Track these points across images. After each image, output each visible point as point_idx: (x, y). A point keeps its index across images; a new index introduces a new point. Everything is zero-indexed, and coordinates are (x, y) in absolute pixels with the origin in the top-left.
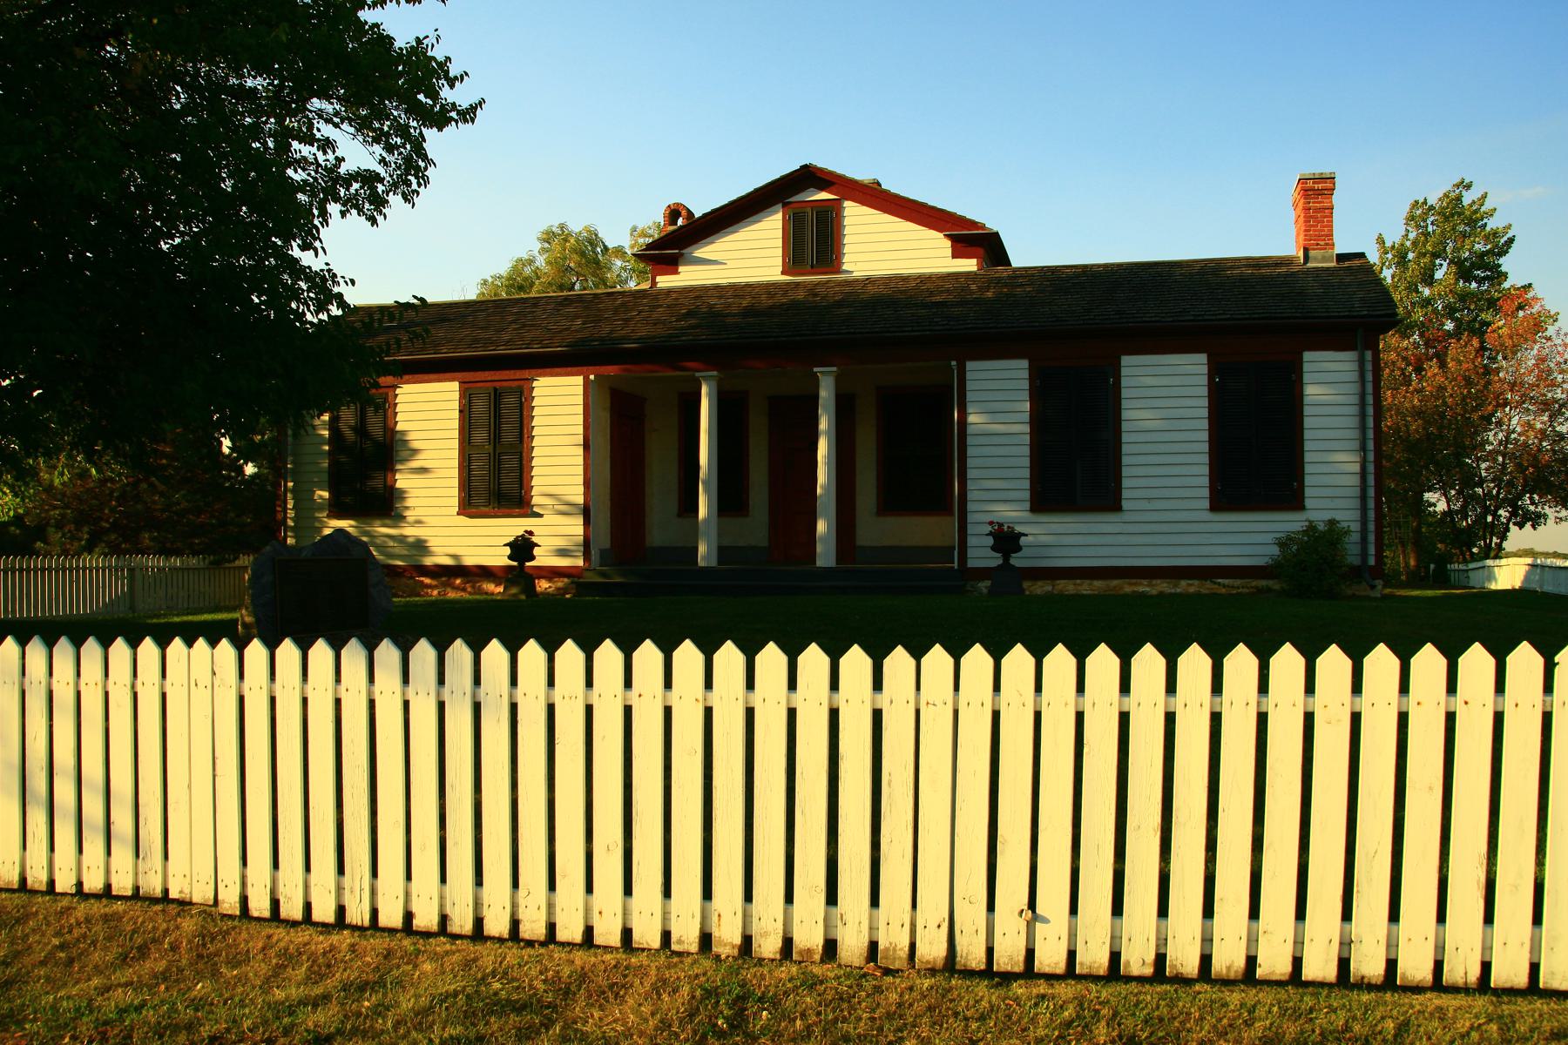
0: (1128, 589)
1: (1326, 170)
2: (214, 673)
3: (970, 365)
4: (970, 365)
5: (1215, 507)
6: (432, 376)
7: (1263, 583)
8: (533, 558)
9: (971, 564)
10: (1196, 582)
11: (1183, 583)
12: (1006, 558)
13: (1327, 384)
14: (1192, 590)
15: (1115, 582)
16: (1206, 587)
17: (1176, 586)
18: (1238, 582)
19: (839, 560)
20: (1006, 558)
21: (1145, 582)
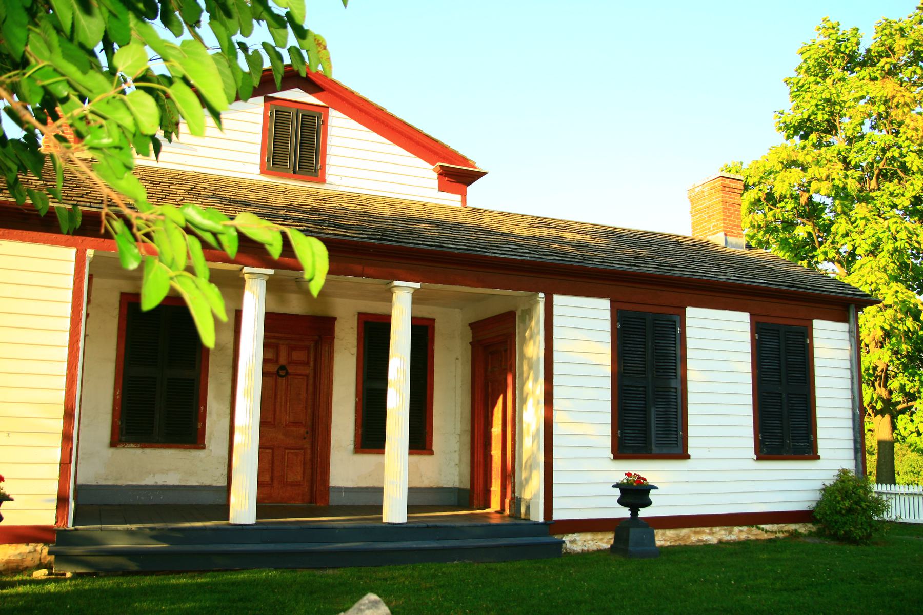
0: (694, 538)
1: (113, 450)
2: (9, 433)
3: (558, 299)
4: (558, 299)
5: (759, 458)
6: (16, 232)
7: (792, 527)
8: (648, 503)
9: (557, 516)
10: (745, 528)
11: (736, 529)
12: (634, 512)
13: (828, 341)
14: (743, 536)
15: (684, 532)
16: (739, 533)
17: (730, 533)
18: (775, 527)
19: (259, 515)
20: (634, 512)
21: (707, 530)
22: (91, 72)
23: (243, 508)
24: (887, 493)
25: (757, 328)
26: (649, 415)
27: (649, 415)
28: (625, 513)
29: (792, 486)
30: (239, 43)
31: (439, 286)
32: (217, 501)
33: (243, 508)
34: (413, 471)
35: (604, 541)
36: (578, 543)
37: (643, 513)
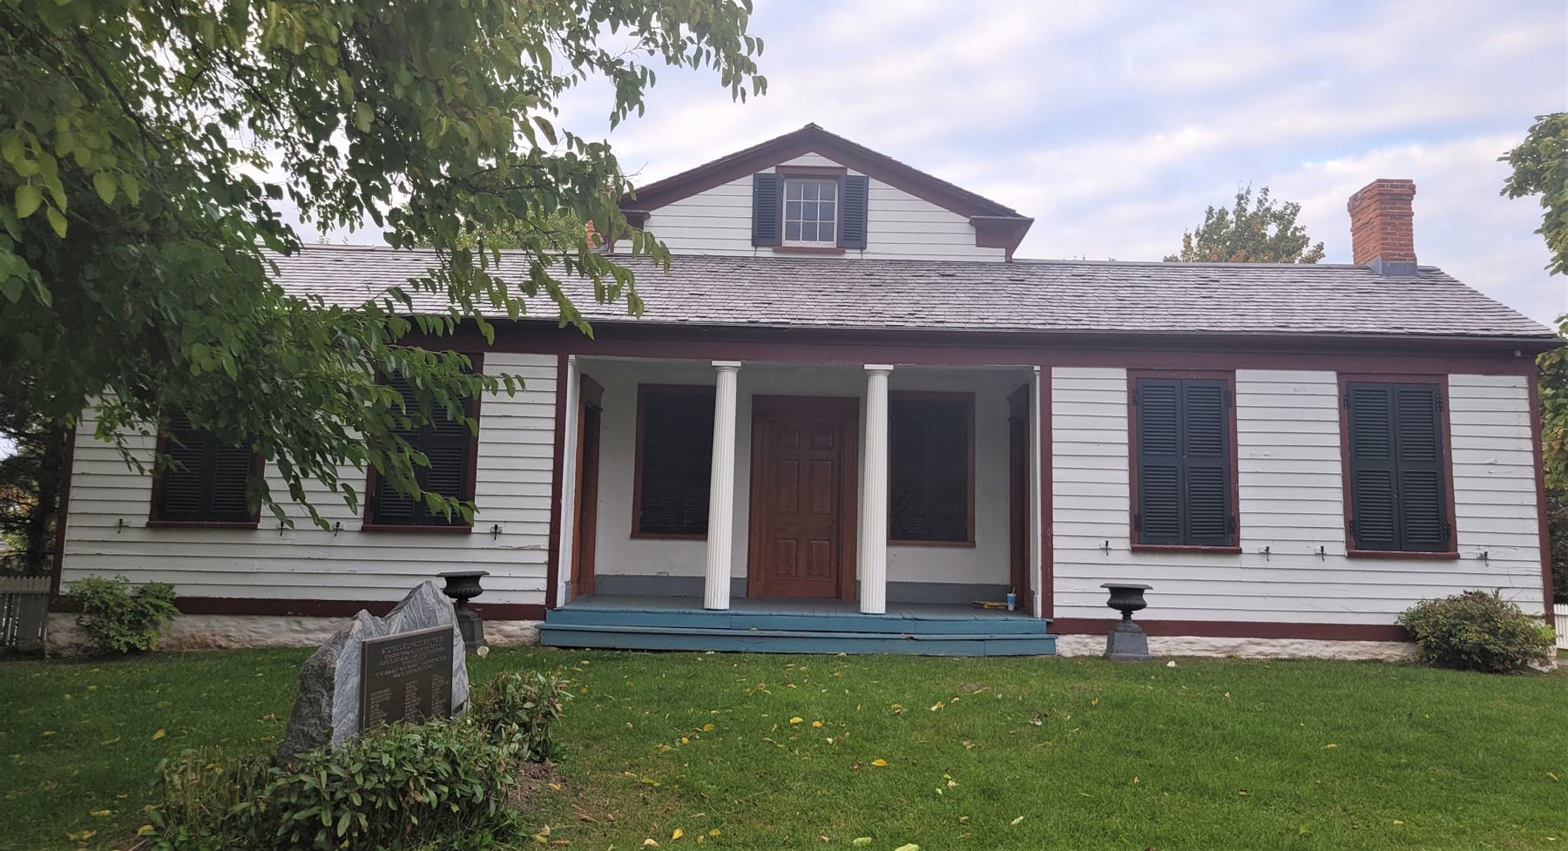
3: (1056, 372)
4: (1056, 372)
12: (1127, 615)
20: (1127, 615)
22: (1509, 170)
23: (719, 596)
24: (24, 595)
25: (1350, 403)
26: (1186, 501)
27: (1186, 501)
28: (1117, 615)
29: (1399, 589)
30: (538, 119)
31: (599, 357)
32: (694, 589)
33: (719, 596)
34: (704, 558)
35: (1097, 645)
36: (1067, 645)
37: (1137, 615)
